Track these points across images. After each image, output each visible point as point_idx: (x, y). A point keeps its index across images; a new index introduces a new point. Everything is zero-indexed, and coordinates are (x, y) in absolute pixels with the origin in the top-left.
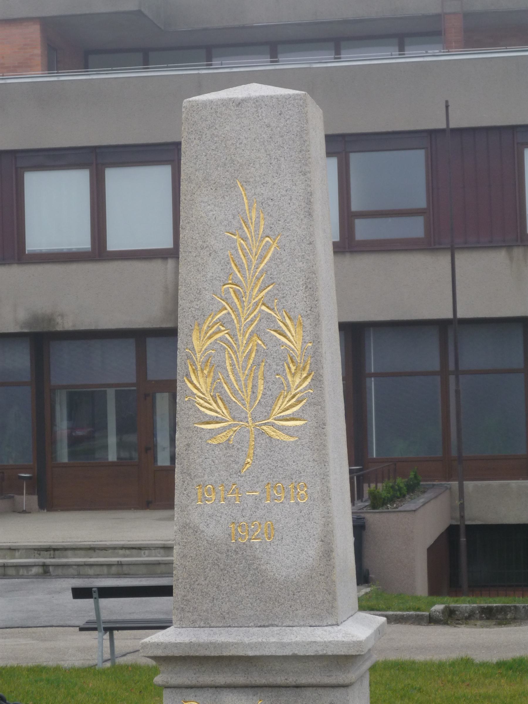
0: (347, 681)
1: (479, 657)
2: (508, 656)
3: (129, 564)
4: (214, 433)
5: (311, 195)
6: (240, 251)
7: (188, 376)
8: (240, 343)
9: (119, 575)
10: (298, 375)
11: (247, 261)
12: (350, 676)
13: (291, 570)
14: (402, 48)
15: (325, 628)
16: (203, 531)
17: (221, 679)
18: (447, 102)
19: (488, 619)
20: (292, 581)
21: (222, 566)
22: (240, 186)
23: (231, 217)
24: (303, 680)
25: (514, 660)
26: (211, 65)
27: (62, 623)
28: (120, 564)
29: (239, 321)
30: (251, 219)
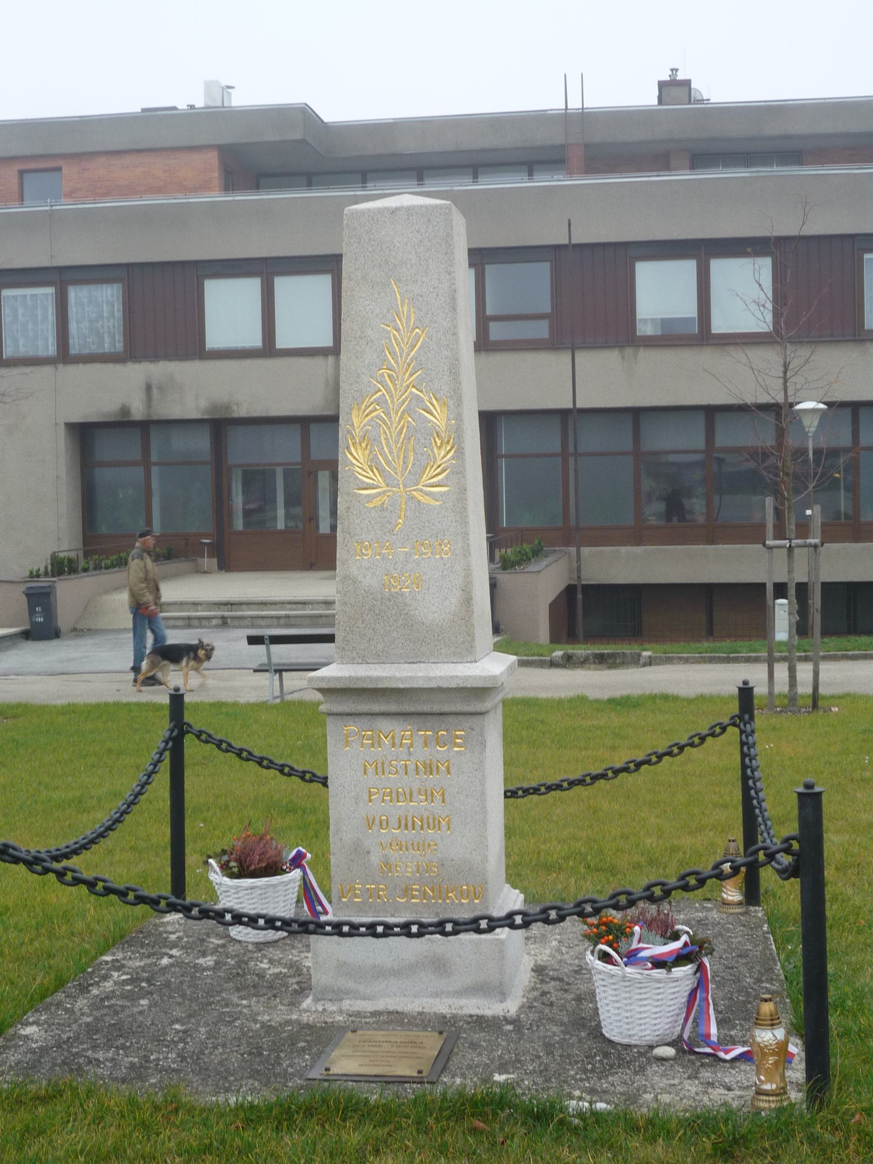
0: (483, 710)
1: (592, 694)
2: (617, 694)
3: (296, 617)
4: (370, 498)
5: (455, 292)
6: (393, 340)
7: (348, 448)
8: (393, 420)
9: (287, 626)
10: (444, 448)
11: (399, 349)
12: (488, 705)
13: (436, 615)
14: (531, 174)
15: (466, 664)
16: (361, 582)
17: (376, 708)
18: (569, 221)
19: (600, 663)
20: (438, 624)
21: (377, 612)
22: (393, 283)
23: (386, 310)
24: (446, 708)
25: (622, 697)
26: (366, 187)
27: (239, 666)
28: (288, 617)
29: (392, 402)
30: (403, 312)
